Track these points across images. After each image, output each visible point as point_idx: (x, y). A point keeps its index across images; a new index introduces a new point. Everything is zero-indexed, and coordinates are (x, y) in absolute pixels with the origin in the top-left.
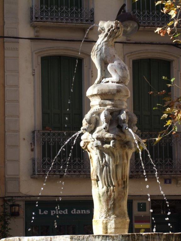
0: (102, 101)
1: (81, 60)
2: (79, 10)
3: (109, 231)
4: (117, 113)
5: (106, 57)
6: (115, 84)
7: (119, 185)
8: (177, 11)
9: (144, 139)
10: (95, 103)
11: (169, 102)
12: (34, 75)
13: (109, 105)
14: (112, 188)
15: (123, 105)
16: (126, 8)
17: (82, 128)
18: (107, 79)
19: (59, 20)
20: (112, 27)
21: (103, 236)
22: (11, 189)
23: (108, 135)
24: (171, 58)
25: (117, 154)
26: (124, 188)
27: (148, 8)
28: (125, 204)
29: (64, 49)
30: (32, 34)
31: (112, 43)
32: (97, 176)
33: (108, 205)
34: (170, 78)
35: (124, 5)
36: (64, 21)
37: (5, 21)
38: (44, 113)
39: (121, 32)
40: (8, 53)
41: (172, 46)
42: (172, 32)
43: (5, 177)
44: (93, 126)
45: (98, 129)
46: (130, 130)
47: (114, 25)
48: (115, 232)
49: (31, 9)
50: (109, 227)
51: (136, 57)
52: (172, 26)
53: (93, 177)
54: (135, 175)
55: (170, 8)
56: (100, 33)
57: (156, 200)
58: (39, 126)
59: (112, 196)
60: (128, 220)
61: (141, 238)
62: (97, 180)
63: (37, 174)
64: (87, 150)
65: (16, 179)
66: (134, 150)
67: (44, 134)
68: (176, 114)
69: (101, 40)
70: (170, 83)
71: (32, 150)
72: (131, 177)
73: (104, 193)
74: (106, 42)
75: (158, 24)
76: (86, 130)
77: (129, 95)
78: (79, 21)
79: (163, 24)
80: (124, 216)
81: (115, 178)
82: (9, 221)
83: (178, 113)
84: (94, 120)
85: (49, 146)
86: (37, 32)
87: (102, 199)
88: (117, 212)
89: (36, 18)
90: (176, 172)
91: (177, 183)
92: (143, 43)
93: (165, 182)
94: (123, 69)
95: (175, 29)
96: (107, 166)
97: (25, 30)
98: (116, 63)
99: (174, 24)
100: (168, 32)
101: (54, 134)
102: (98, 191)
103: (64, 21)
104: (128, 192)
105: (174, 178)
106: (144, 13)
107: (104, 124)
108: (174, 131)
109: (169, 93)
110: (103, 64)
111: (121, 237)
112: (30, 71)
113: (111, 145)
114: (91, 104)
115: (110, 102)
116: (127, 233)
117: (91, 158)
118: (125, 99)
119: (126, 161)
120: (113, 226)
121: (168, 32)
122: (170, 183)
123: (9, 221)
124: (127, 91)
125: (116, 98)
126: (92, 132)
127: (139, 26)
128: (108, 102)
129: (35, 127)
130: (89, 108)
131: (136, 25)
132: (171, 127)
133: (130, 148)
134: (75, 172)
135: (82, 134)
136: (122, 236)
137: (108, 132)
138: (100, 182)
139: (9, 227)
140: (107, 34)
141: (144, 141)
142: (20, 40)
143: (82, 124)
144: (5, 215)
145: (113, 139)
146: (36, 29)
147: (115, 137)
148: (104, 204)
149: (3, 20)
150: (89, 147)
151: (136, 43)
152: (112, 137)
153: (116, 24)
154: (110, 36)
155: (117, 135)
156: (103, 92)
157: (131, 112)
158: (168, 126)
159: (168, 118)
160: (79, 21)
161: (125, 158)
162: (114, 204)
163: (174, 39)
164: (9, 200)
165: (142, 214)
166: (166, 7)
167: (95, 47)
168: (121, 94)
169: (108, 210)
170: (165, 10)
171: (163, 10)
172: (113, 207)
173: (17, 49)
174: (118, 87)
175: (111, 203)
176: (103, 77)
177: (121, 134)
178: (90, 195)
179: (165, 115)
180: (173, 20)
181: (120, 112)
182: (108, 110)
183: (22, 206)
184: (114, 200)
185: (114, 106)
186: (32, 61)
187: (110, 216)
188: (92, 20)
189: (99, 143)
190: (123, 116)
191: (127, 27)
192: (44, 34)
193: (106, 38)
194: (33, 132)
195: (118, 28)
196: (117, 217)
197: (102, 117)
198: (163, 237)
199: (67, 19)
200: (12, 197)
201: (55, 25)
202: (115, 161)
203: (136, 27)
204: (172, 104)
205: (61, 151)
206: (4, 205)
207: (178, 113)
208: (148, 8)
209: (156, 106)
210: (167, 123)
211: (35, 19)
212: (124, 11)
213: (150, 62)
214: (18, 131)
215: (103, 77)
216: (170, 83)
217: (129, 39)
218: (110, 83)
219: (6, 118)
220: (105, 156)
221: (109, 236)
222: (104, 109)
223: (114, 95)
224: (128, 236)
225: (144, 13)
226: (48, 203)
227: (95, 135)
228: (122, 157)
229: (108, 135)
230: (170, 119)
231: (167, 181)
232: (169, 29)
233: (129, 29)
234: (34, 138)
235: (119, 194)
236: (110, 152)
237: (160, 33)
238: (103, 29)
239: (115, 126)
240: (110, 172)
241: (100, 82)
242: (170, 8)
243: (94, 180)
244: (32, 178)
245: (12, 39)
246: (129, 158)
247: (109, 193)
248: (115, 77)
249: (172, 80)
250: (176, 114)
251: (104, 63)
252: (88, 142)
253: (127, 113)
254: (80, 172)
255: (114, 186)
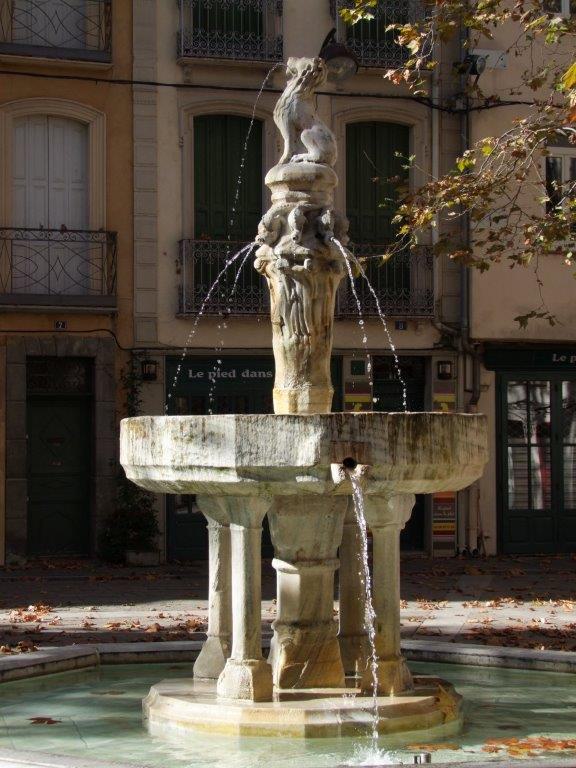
0: (291, 193)
1: (259, 123)
2: (258, 38)
3: (300, 408)
4: (316, 213)
5: (299, 118)
6: (314, 164)
7: (317, 332)
8: (421, 41)
9: (362, 256)
10: (279, 196)
11: (404, 196)
12: (181, 147)
13: (303, 199)
14: (305, 337)
15: (326, 200)
16: (337, 36)
17: (257, 238)
18: (301, 156)
19: (208, 54)
20: (309, 68)
21: (289, 416)
22: (143, 336)
23: (300, 250)
24: (411, 121)
25: (314, 280)
26: (326, 337)
27: (373, 36)
28: (326, 364)
29: (233, 104)
30: (179, 78)
31: (308, 95)
32: (282, 318)
33: (298, 366)
34: (407, 154)
35: (334, 31)
36: (233, 56)
37: (135, 55)
38: (198, 211)
39: (325, 73)
40: (138, 110)
41: (413, 101)
42: (411, 78)
43: (133, 315)
44: (275, 234)
45: (284, 239)
46: (336, 241)
47: (312, 64)
48: (310, 411)
49: (179, 34)
50: (299, 401)
51: (352, 118)
52: (412, 68)
53: (275, 319)
54: (345, 315)
55: (409, 37)
56: (289, 77)
57: (380, 357)
58: (189, 233)
59: (306, 352)
60: (331, 391)
61: (351, 420)
62: (282, 325)
63: (184, 312)
64: (264, 274)
65: (152, 319)
66: (342, 275)
67: (197, 246)
68: (416, 215)
69: (291, 89)
70: (407, 163)
71: (179, 272)
72: (339, 318)
73: (292, 346)
74: (298, 92)
75: (390, 63)
76: (263, 241)
77: (337, 184)
78: (258, 57)
79: (398, 63)
80: (325, 385)
81: (311, 321)
82: (140, 388)
83: (419, 214)
84: (276, 225)
85: (206, 266)
86: (187, 74)
87: (288, 355)
88: (313, 377)
89: (187, 50)
90: (415, 310)
91: (416, 328)
92: (364, 96)
93: (397, 328)
94: (326, 139)
95: (416, 73)
96: (297, 300)
97: (167, 72)
98: (315, 128)
99: (415, 65)
100: (406, 78)
101: (214, 247)
102: (281, 342)
103: (233, 56)
104: (331, 344)
105: (411, 320)
106: (366, 45)
107: (293, 232)
108: (412, 243)
109: (405, 181)
110: (294, 131)
111: (319, 419)
112: (175, 139)
113: (305, 266)
114: (273, 197)
115: (305, 195)
116: (329, 412)
117: (271, 287)
118: (330, 190)
119: (329, 293)
120: (307, 400)
121: (406, 78)
122: (405, 328)
123: (140, 388)
124: (333, 176)
125: (315, 188)
126: (273, 245)
127: (358, 66)
128: (300, 194)
129: (183, 234)
130: (270, 204)
131: (352, 64)
132: (408, 237)
133: (337, 272)
134: (248, 309)
135: (256, 248)
136: (321, 416)
137: (300, 244)
138: (286, 328)
139: (139, 398)
140: (300, 80)
141: (362, 259)
142: (159, 88)
143: (257, 231)
144: (133, 377)
145: (309, 256)
146: (186, 69)
147: (312, 253)
148: (292, 364)
149: (132, 53)
150: (269, 268)
151: (351, 95)
152: (306, 253)
153: (317, 62)
154: (305, 84)
155: (315, 250)
156: (294, 177)
157: (342, 211)
158: (402, 235)
159: (404, 222)
160: (258, 57)
161: (329, 288)
162: (309, 364)
163: (416, 88)
164: (140, 354)
165: (359, 378)
166: (403, 35)
167: (280, 102)
168: (323, 181)
169: (299, 374)
170: (401, 40)
171: (397, 40)
172: (305, 368)
173: (154, 103)
174: (317, 169)
175: (304, 362)
176: (293, 152)
177: (322, 249)
178: (268, 346)
179: (399, 217)
180: (414, 57)
181: (321, 211)
182: (300, 208)
183: (161, 365)
184: (309, 357)
185: (310, 201)
186: (179, 121)
187: (301, 383)
188: (280, 56)
189: (286, 263)
190: (326, 219)
191: (338, 68)
192: (199, 78)
193: (299, 87)
194: (180, 242)
195: (319, 70)
196: (314, 385)
197: (291, 220)
198: (389, 419)
199: (238, 54)
200: (145, 349)
201: (196, 60)
202: (311, 293)
203: (352, 69)
204: (409, 199)
205: (212, 283)
206: (131, 361)
207: (420, 214)
208: (373, 36)
209: (383, 202)
210: (400, 230)
211: (184, 54)
212: (334, 41)
213: (374, 127)
214: (155, 241)
215: (293, 152)
216: (407, 163)
217: (340, 87)
218: (305, 162)
219: (136, 219)
220: (295, 285)
221: (298, 417)
222: (294, 206)
223: (311, 182)
224: (331, 416)
225: (366, 45)
226: (201, 360)
227: (278, 249)
228: (322, 287)
229: (300, 250)
230: (407, 223)
231: (399, 326)
232: (407, 71)
233: (341, 70)
234: (181, 252)
235: (317, 348)
236: (303, 278)
237: (392, 79)
238: (294, 71)
239: (312, 235)
240: (302, 312)
241: (288, 161)
242: (409, 37)
243: (276, 323)
244: (178, 318)
245: (49, 74)
246: (336, 287)
247: (300, 346)
248: (312, 153)
249: (411, 159)
250: (416, 215)
251: (295, 129)
252: (267, 262)
253: (332, 212)
254: (256, 308)
255: (308, 335)
